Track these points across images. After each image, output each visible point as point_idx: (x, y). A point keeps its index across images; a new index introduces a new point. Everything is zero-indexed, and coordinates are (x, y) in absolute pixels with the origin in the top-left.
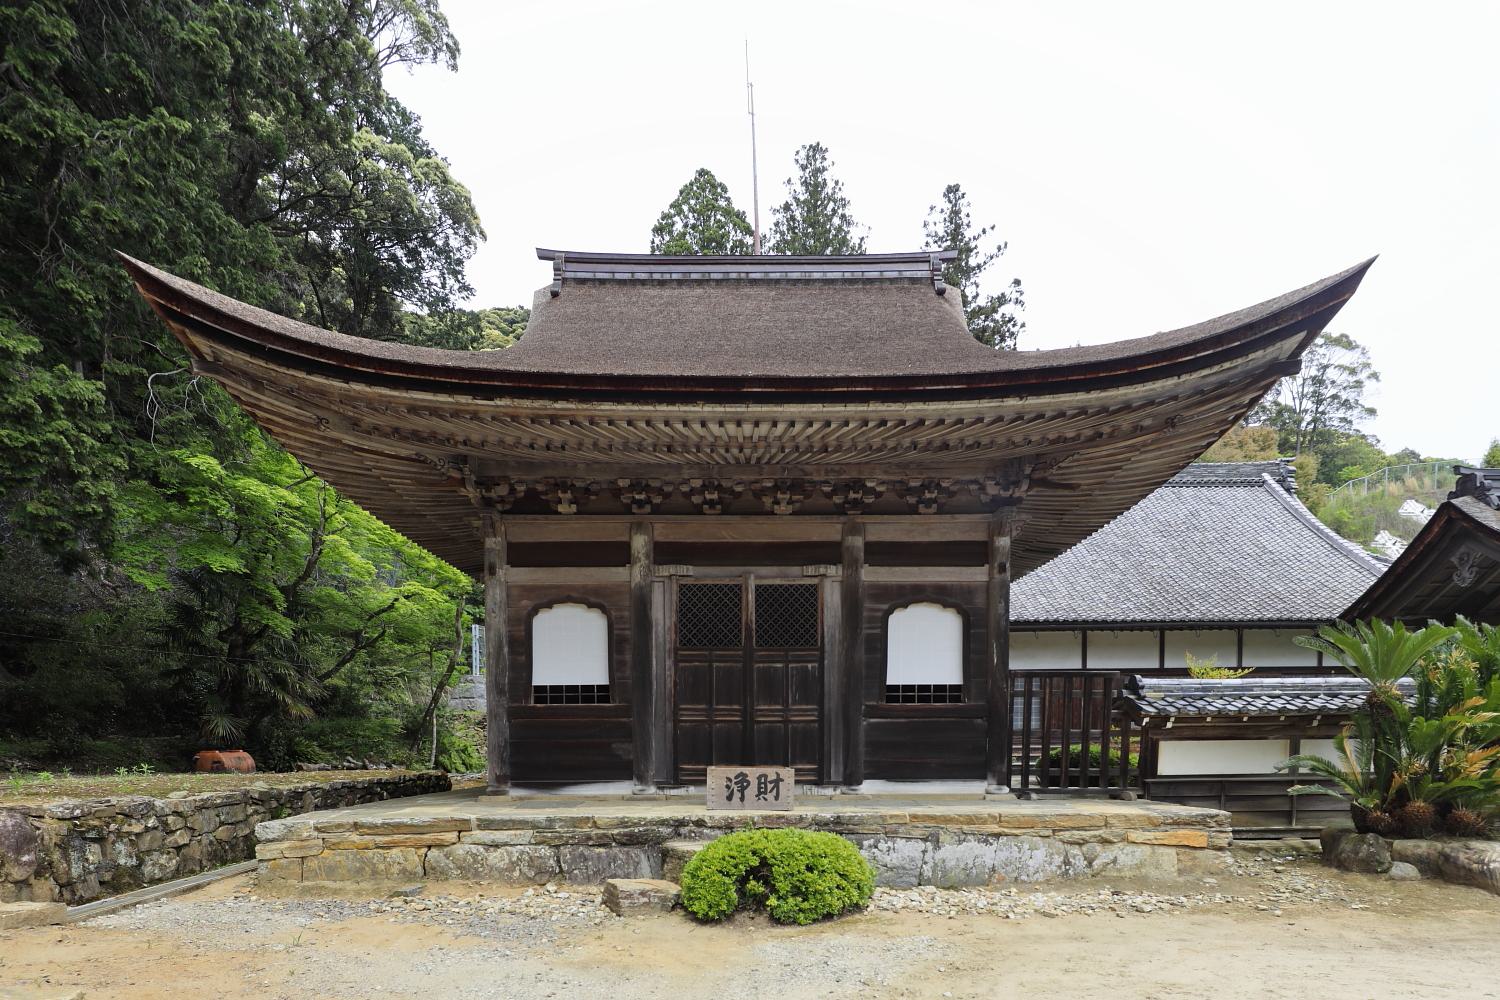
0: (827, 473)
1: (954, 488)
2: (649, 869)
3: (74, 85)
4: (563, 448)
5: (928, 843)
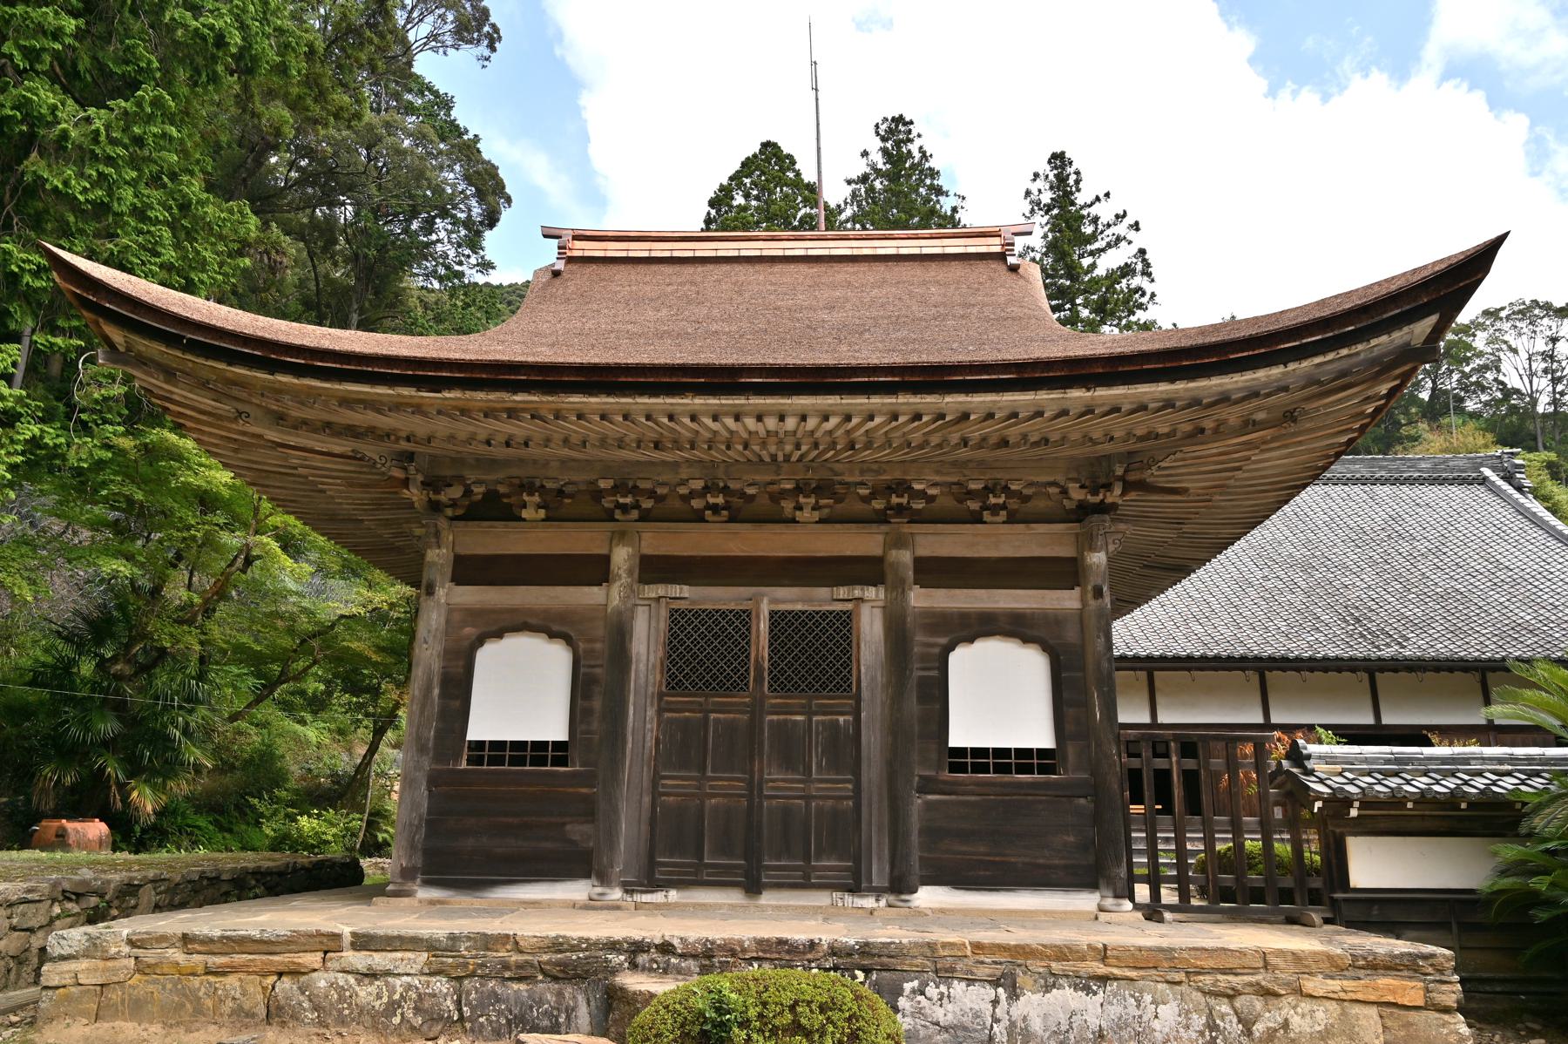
0: (862, 472)
1: (1027, 492)
2: (587, 1019)
3: (67, 78)
4: (526, 444)
5: (1000, 990)
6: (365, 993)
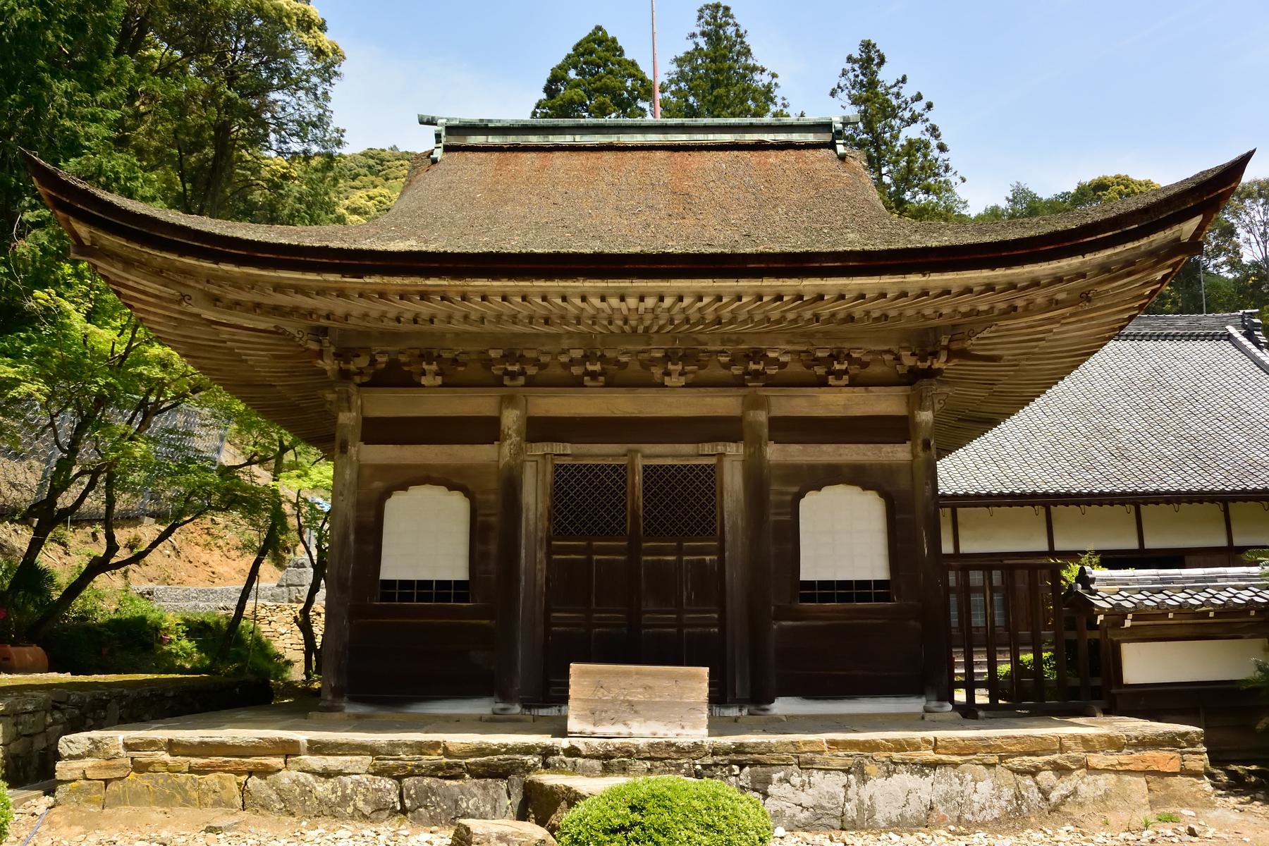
1: (867, 359)
4: (432, 321)
5: (851, 776)
6: (323, 788)
